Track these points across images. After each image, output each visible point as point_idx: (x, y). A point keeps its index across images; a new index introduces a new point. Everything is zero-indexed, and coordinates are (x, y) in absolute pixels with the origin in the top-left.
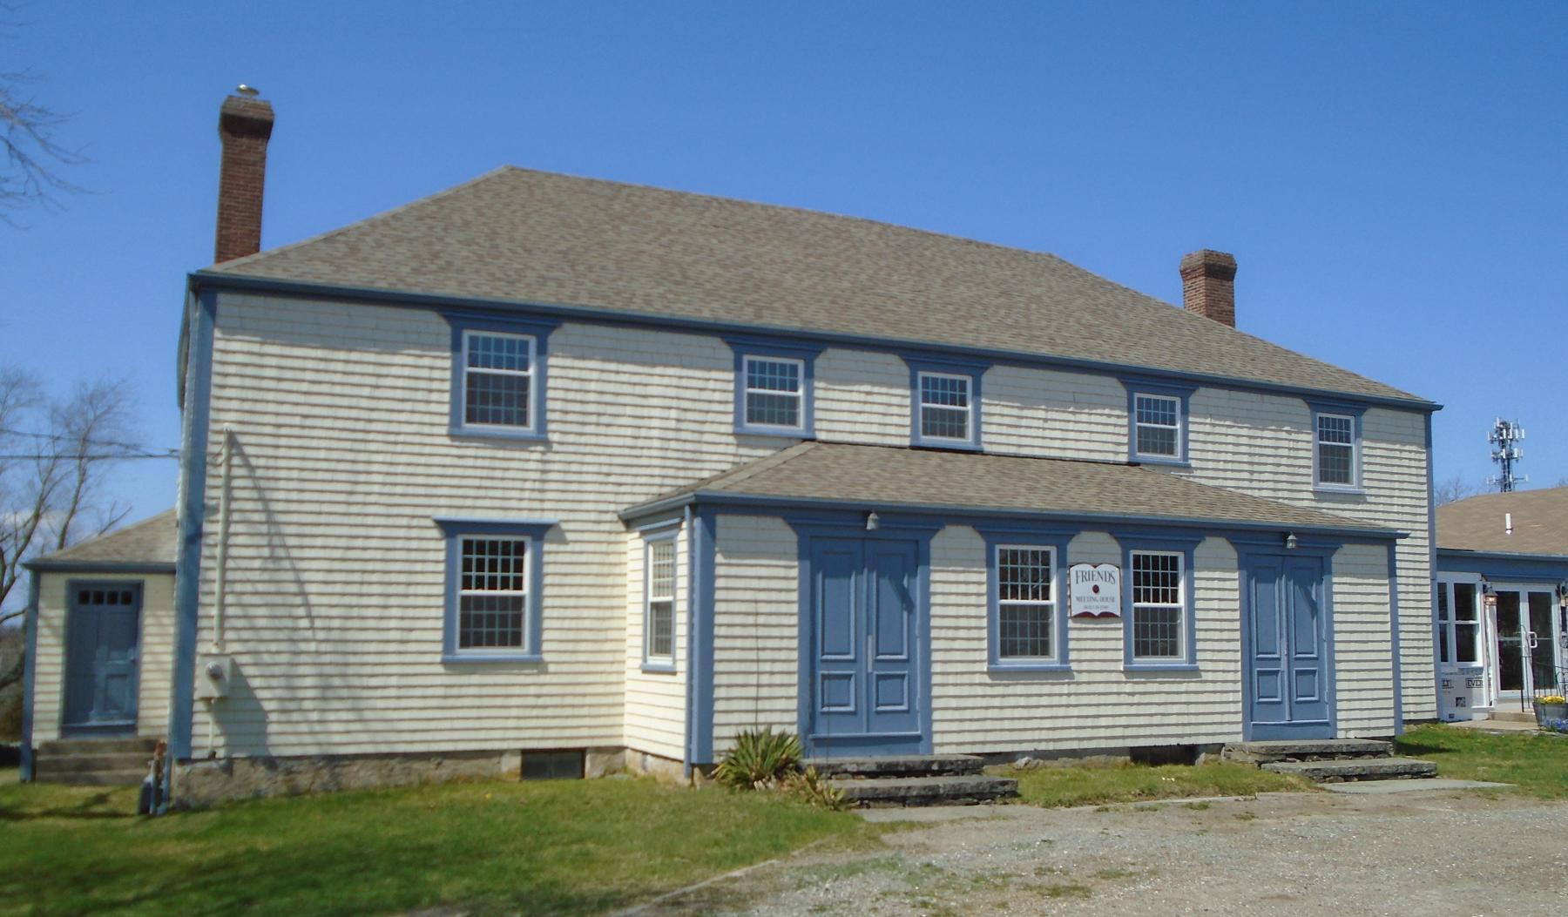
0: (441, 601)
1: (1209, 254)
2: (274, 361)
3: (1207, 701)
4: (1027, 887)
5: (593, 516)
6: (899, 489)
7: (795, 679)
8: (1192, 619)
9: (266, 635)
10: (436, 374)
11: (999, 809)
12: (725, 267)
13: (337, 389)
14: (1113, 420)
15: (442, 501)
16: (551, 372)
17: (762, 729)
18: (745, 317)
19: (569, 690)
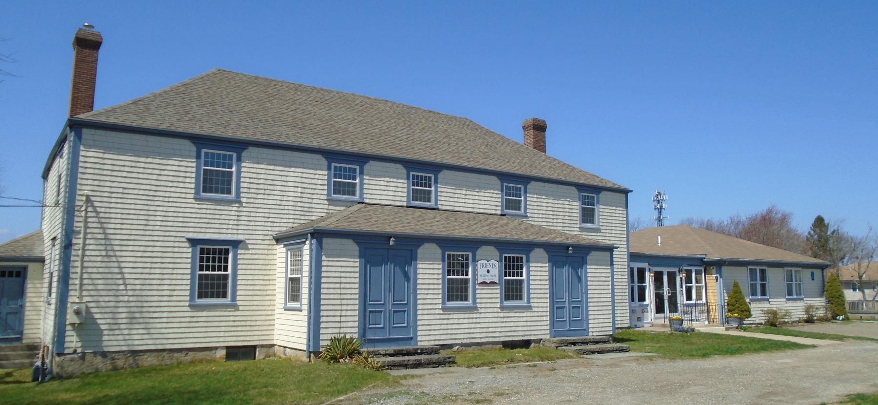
0: (189, 277)
1: (535, 120)
2: (110, 162)
3: (534, 321)
4: (466, 400)
5: (261, 237)
6: (403, 226)
7: (357, 313)
8: (529, 284)
9: (103, 293)
10: (189, 169)
11: (448, 369)
12: (322, 121)
13: (141, 176)
14: (494, 195)
15: (191, 230)
16: (243, 170)
17: (342, 335)
18: (332, 145)
19: (249, 318)
